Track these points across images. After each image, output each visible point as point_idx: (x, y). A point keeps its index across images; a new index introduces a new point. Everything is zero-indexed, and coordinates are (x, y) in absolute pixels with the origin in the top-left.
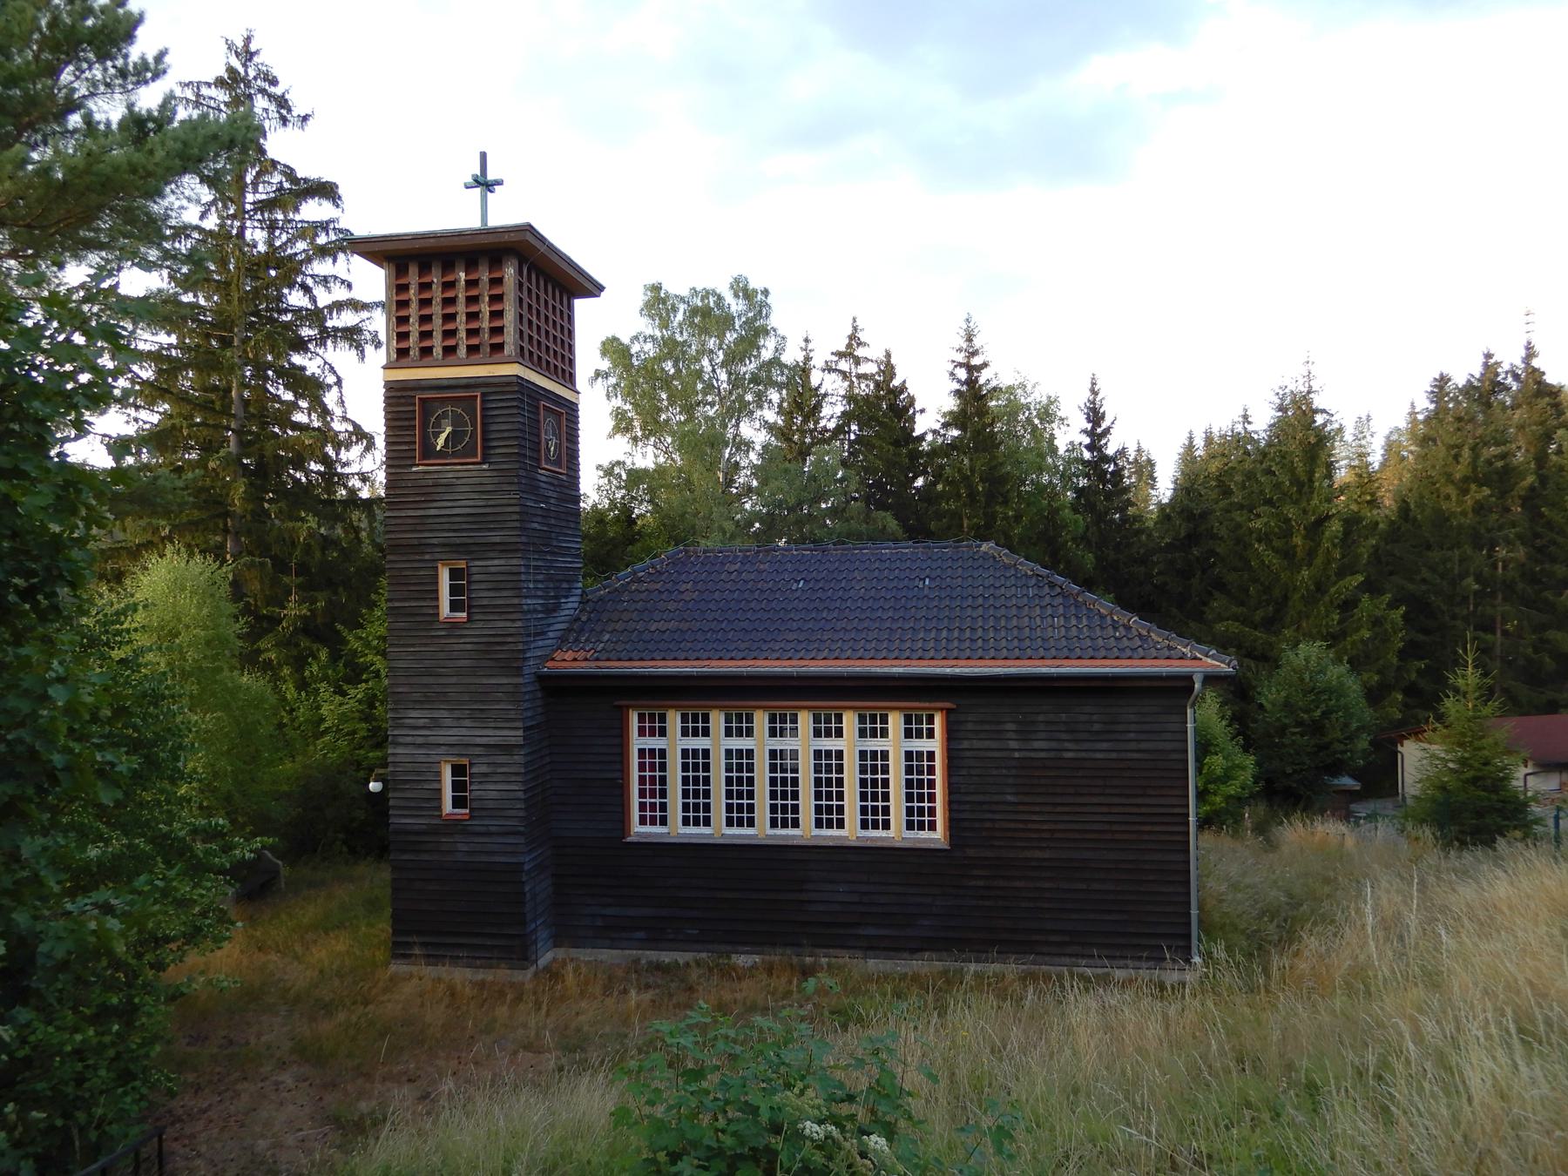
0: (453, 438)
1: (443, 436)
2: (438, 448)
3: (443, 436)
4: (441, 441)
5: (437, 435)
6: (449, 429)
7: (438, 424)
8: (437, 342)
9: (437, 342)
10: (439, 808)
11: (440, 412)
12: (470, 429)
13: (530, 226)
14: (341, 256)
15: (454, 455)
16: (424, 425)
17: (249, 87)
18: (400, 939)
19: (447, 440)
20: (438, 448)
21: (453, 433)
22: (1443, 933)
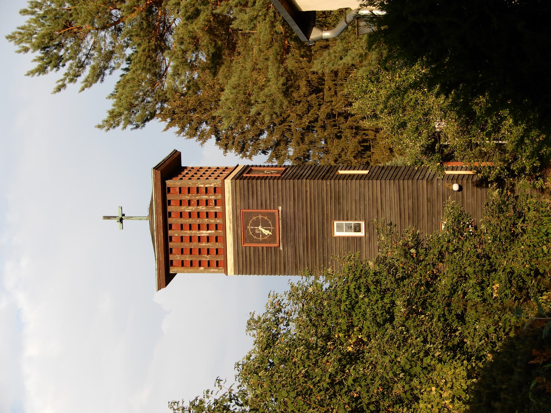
0: (265, 225)
1: (263, 230)
2: (271, 233)
3: (263, 230)
4: (267, 232)
5: (264, 235)
6: (260, 228)
7: (258, 235)
8: (212, 245)
9: (212, 245)
10: (360, 238)
11: (251, 233)
12: (260, 217)
13: (156, 168)
14: (345, 353)
15: (274, 225)
16: (259, 242)
17: (420, 118)
18: (264, 207)
19: (266, 229)
20: (271, 233)
21: (263, 226)
22: (532, 362)
